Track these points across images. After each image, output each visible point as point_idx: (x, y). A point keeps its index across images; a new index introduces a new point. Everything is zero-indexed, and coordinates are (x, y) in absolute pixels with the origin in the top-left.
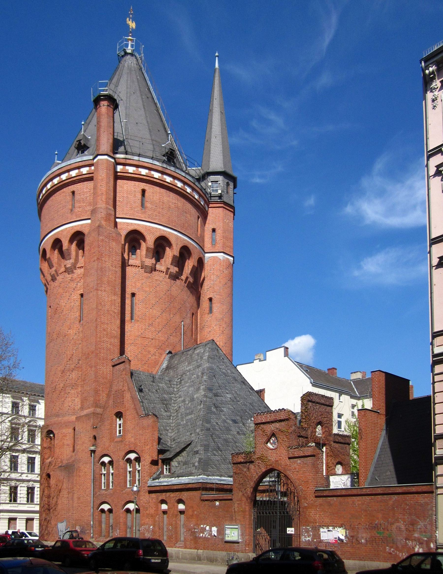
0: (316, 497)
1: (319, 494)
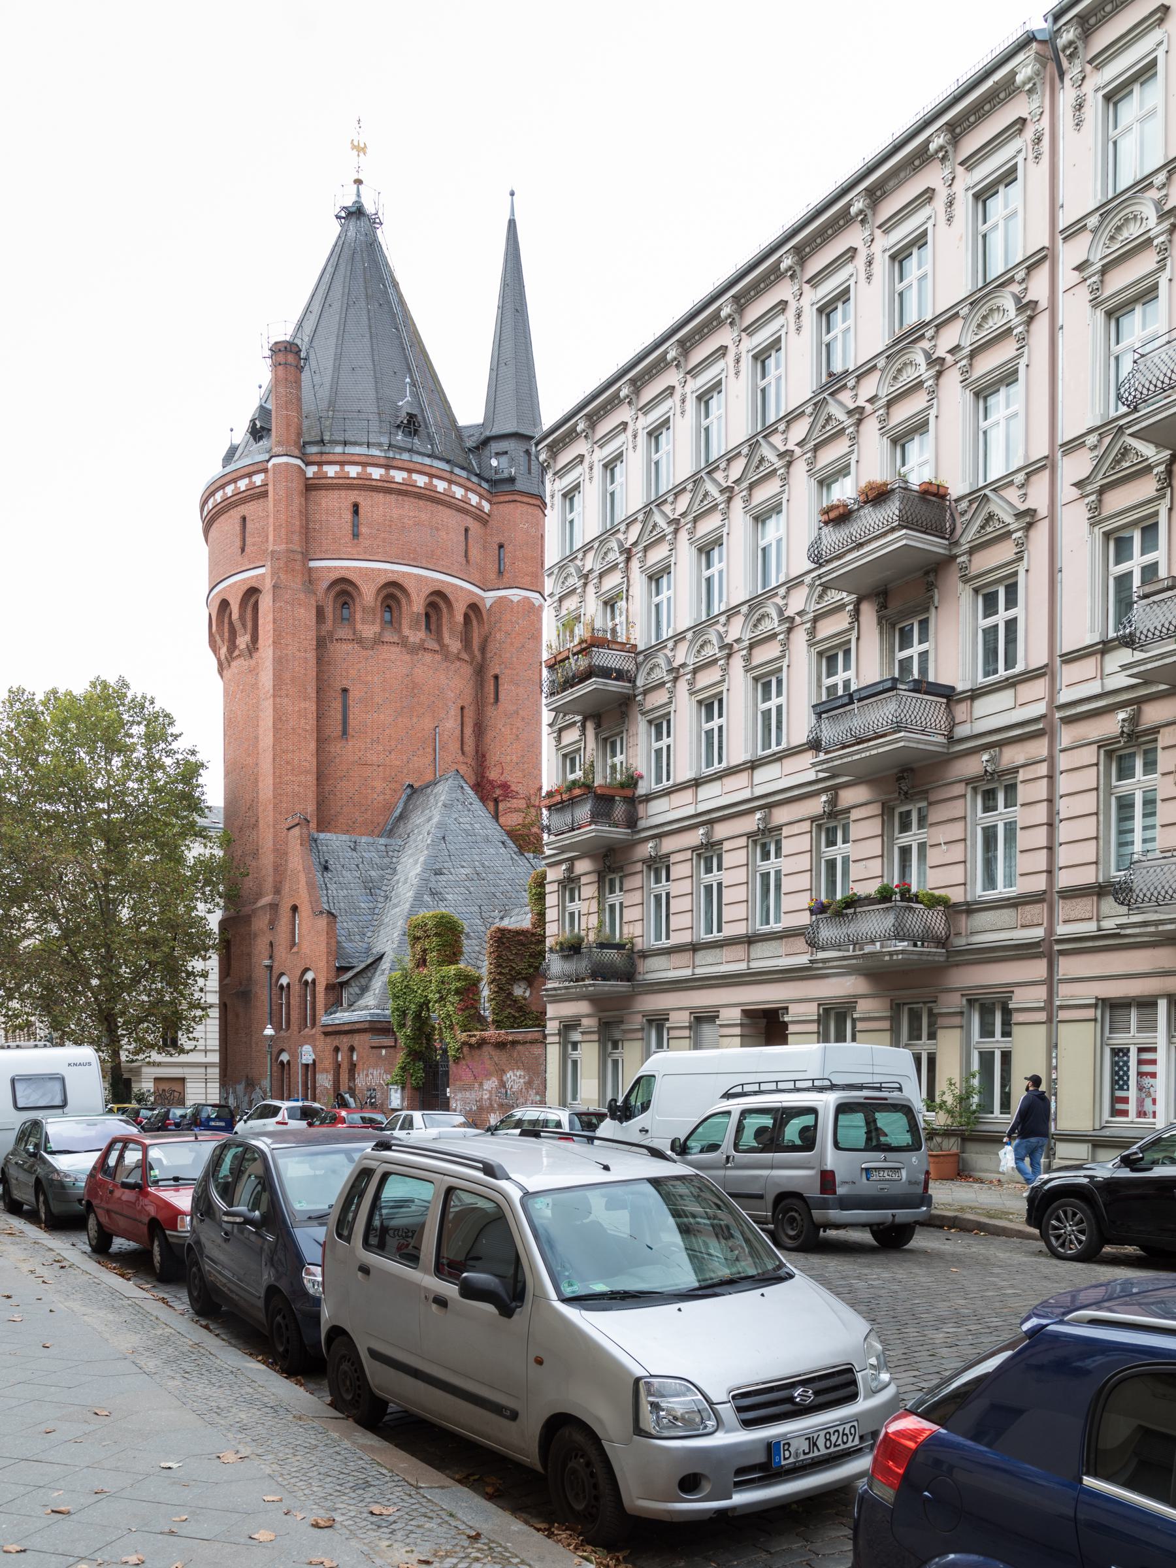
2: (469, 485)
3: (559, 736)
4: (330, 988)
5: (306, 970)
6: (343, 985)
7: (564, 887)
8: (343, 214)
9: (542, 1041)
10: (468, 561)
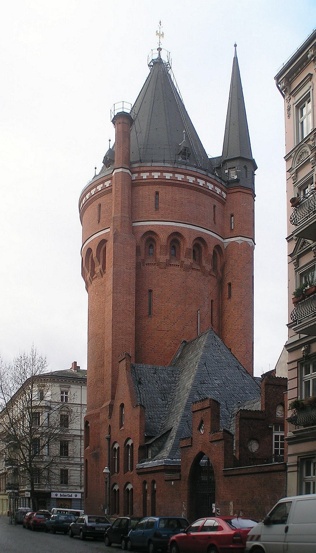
0: (225, 476)
1: (228, 473)
2: (216, 183)
3: (298, 262)
4: (141, 448)
5: (128, 439)
6: (149, 446)
7: (302, 365)
8: (152, 64)
9: (284, 470)
10: (215, 223)
